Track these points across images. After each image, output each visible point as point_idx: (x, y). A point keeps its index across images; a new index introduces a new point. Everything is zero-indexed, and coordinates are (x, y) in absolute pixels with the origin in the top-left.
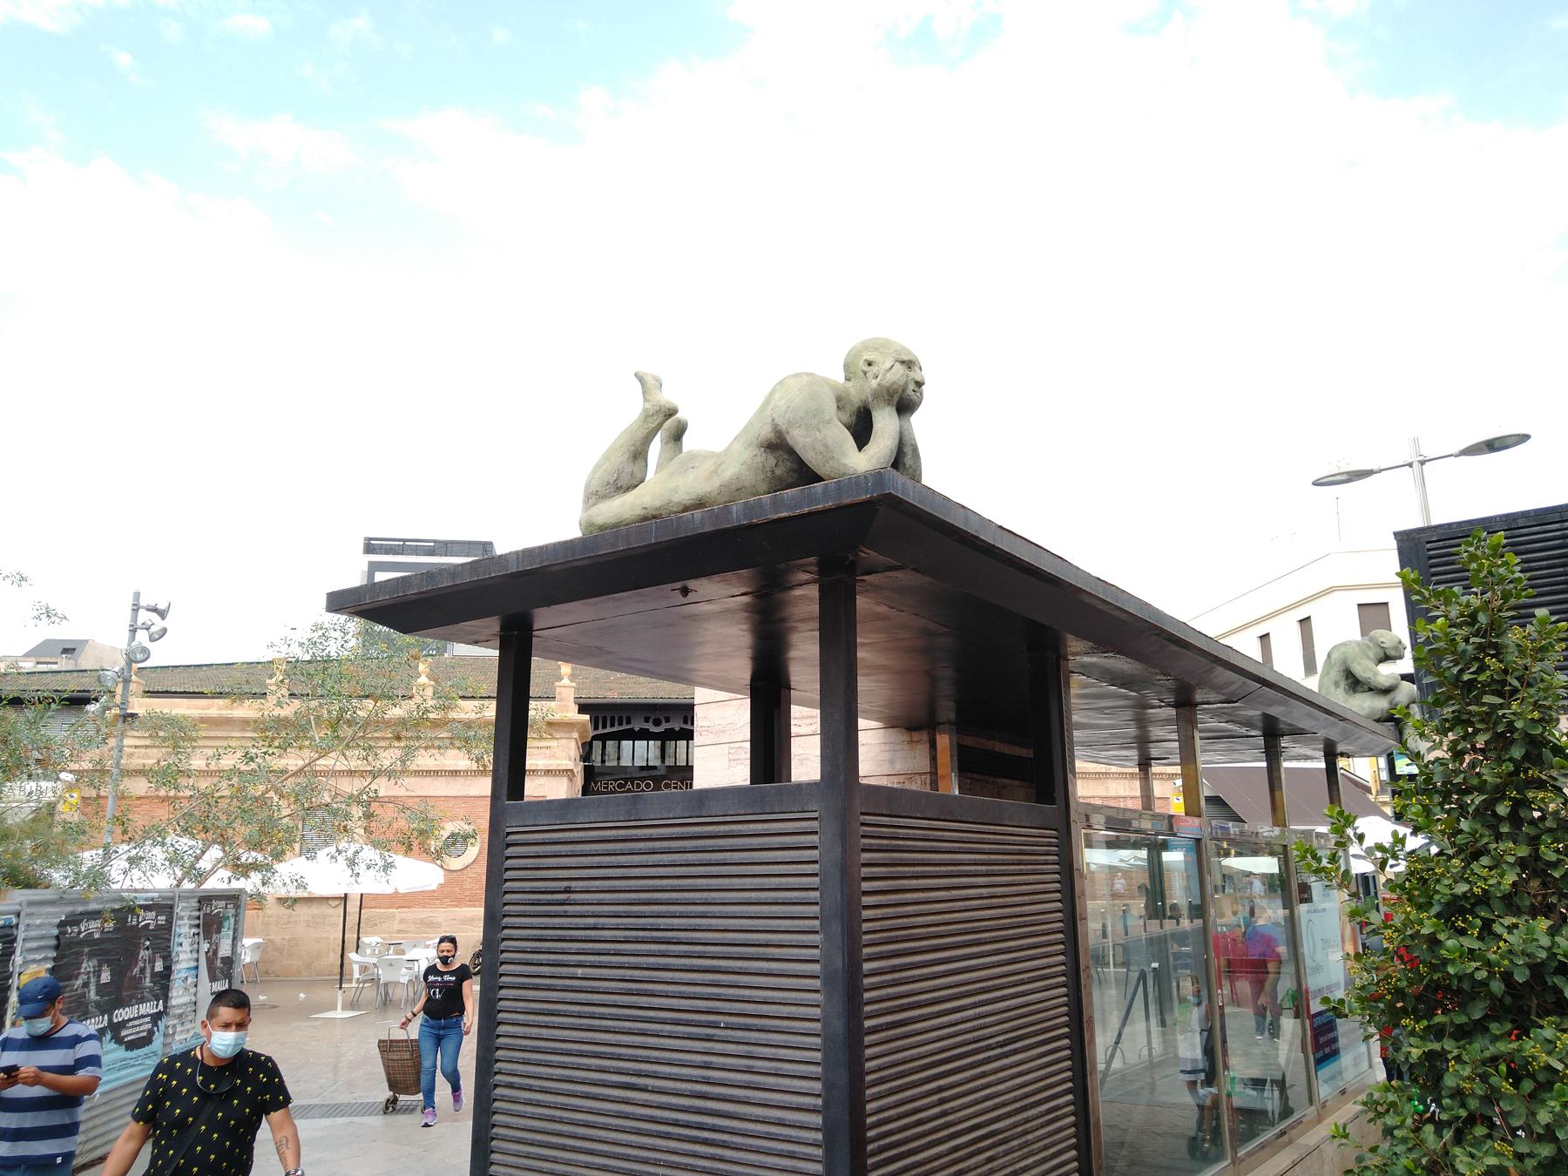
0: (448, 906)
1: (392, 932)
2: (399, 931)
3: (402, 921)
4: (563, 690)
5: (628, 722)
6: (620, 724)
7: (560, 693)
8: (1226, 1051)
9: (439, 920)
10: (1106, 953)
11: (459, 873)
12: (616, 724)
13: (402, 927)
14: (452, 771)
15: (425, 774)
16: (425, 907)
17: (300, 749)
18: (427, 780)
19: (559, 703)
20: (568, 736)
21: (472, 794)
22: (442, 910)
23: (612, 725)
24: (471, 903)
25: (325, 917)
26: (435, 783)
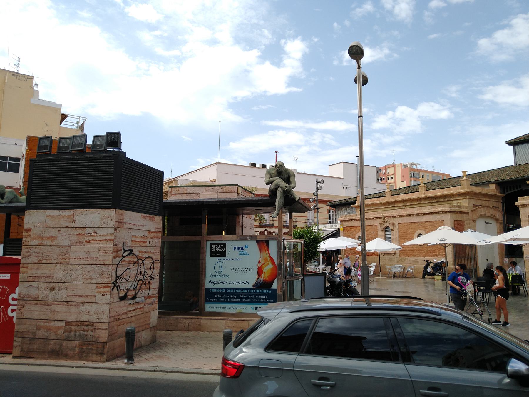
0: (421, 256)
1: (407, 264)
2: (409, 264)
3: (409, 260)
4: (463, 181)
5: (520, 187)
6: (514, 189)
7: (462, 183)
8: (144, 370)
9: (419, 260)
10: (380, 321)
11: (423, 246)
12: (512, 189)
13: (409, 262)
14: (417, 214)
15: (521, 206)
16: (415, 257)
17: (34, 239)
18: (411, 217)
19: (462, 186)
20: (465, 198)
21: (423, 221)
22: (419, 257)
23: (517, 188)
24: (427, 256)
25: (392, 258)
26: (413, 218)
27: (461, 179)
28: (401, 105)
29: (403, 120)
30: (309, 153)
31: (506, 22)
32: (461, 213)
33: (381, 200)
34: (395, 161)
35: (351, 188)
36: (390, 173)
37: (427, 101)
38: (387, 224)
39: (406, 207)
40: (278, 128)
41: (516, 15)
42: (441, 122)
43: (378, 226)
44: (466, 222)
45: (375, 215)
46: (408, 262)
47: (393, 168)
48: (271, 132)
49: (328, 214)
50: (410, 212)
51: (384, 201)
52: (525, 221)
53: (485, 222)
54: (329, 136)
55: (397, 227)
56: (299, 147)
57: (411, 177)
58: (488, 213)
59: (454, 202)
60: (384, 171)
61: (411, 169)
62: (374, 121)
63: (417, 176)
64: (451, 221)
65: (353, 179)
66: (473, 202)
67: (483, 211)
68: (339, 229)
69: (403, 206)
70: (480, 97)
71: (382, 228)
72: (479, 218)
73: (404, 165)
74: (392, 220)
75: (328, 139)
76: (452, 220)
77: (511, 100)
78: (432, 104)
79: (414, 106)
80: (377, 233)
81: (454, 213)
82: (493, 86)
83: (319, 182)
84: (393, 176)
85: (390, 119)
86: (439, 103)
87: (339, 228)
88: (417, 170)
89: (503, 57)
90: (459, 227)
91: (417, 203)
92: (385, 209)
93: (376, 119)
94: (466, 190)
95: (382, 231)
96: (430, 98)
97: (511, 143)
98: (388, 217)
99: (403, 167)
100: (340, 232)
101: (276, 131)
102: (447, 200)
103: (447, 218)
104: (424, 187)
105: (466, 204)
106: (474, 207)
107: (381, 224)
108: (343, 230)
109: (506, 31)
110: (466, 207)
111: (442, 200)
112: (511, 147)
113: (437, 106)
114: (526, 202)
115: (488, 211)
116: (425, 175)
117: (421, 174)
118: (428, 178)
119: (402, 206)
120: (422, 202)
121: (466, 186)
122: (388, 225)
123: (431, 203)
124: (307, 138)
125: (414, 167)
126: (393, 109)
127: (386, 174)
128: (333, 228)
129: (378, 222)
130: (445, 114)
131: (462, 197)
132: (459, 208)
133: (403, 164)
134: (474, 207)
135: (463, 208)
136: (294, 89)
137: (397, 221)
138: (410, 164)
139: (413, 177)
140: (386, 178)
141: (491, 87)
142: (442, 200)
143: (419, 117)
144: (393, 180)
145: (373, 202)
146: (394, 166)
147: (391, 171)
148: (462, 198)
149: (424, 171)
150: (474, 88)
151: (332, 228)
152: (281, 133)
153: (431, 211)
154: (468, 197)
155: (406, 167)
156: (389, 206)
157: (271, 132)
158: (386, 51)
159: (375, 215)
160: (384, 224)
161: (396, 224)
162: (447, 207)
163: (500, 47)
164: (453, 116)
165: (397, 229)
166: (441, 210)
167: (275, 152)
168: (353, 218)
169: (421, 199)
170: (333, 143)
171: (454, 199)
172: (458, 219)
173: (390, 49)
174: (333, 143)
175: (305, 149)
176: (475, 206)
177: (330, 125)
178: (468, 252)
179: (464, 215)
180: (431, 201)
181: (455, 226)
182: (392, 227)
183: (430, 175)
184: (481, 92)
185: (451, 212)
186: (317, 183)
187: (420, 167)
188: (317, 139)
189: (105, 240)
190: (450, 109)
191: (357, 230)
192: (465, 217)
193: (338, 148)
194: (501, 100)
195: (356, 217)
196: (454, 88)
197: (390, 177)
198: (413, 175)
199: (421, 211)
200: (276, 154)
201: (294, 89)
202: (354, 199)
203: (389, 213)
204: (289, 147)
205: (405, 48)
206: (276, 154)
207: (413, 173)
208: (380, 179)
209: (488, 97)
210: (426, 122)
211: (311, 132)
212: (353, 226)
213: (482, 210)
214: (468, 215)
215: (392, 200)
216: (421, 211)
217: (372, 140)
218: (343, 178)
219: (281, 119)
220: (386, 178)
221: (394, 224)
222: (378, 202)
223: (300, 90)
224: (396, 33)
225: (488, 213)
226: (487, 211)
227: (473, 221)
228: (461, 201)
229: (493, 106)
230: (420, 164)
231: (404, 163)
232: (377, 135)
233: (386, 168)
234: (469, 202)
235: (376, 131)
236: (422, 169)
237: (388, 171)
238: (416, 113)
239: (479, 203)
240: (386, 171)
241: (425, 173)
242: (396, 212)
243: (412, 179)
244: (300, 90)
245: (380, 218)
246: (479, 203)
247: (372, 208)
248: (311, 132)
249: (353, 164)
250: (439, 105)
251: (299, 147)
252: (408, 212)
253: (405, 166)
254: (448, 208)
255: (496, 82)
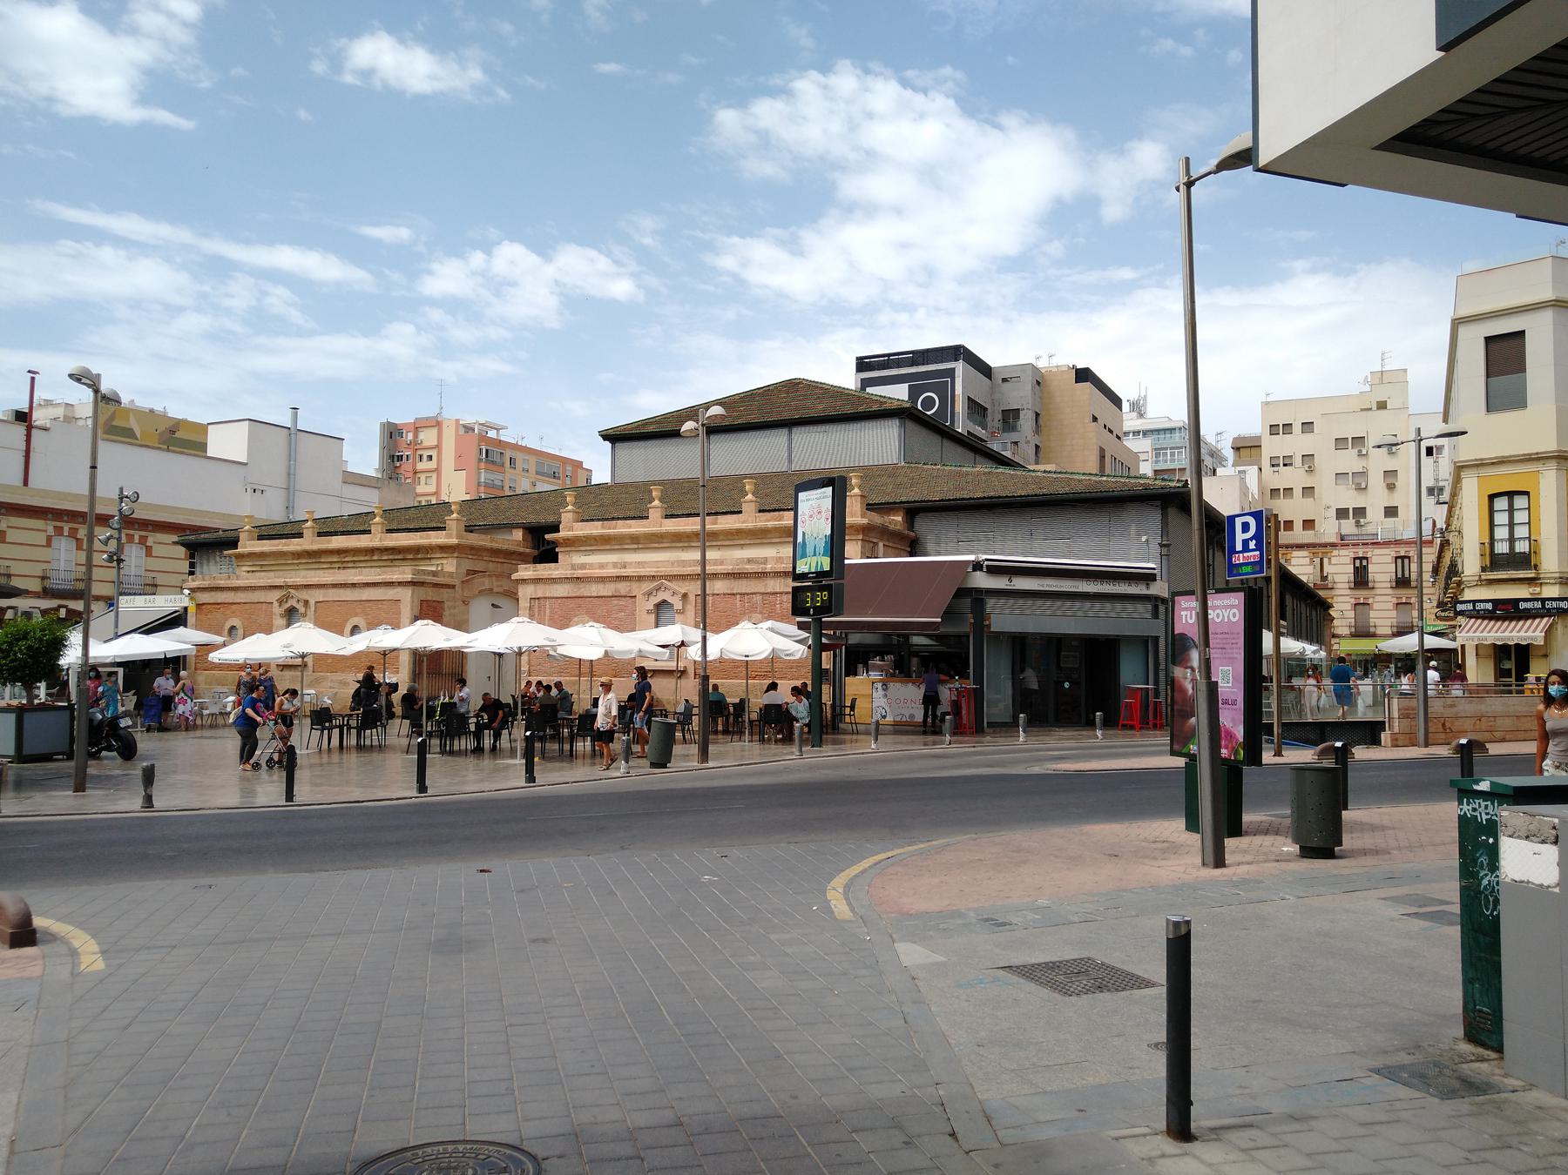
3: (332, 681)
18: (342, 591)
21: (364, 599)
27: (448, 518)
28: (513, 239)
29: (513, 284)
30: (214, 337)
31: (777, 81)
32: (436, 585)
33: (294, 545)
34: (444, 411)
35: (269, 492)
36: (425, 444)
37: (581, 242)
38: (292, 603)
39: (344, 565)
40: (100, 237)
41: (803, 69)
42: (608, 308)
43: (274, 606)
44: (447, 604)
45: (269, 581)
46: (329, 685)
47: (435, 431)
48: (67, 245)
49: (187, 563)
50: (340, 578)
51: (299, 548)
52: (525, 608)
53: (493, 605)
54: (282, 291)
55: (313, 609)
56: (174, 311)
57: (480, 460)
58: (498, 586)
59: (434, 562)
60: (410, 436)
61: (483, 438)
62: (430, 273)
63: (497, 458)
64: (413, 602)
65: (273, 473)
66: (468, 564)
67: (486, 583)
68: (186, 609)
69: (338, 562)
70: (709, 258)
71: (282, 610)
72: (477, 596)
73: (464, 426)
74: (304, 595)
75: (279, 299)
76: (416, 601)
77: (776, 280)
78: (593, 253)
79: (543, 248)
80: (272, 621)
81: (422, 586)
82: (742, 236)
83: (127, 497)
84: (434, 453)
85: (474, 273)
86: (609, 254)
87: (185, 605)
88: (500, 443)
89: (768, 169)
90: (430, 611)
91: (366, 558)
92: (301, 567)
93: (435, 266)
94: (454, 541)
95: (282, 616)
96: (591, 237)
97: (609, 436)
98: (297, 587)
99: (462, 431)
100: (189, 615)
101: (89, 244)
102: (419, 556)
103: (406, 595)
104: (380, 526)
105: (452, 569)
106: (468, 574)
107: (281, 602)
108: (194, 611)
109: (779, 105)
110: (451, 575)
111: (411, 556)
112: (608, 445)
113: (603, 263)
114: (527, 575)
115: (499, 583)
116: (519, 457)
117: (508, 454)
118: (526, 467)
119: (335, 562)
120: (375, 558)
121: (454, 533)
122: (295, 605)
123: (392, 560)
124: (206, 288)
125: (492, 434)
126: (488, 248)
127: (415, 444)
128: (171, 604)
129: (274, 596)
130: (622, 288)
131: (446, 552)
132: (434, 576)
133: (461, 423)
134: (468, 574)
135: (444, 577)
136: (164, 117)
137: (314, 596)
138: (480, 424)
139: (486, 462)
140: (415, 454)
141: (735, 240)
142: (411, 556)
143: (557, 283)
144: (432, 465)
145: (274, 549)
146: (437, 424)
147: (428, 437)
148: (445, 556)
149: (516, 447)
150: (698, 233)
151: (146, 605)
152: (107, 253)
153: (378, 579)
154: (455, 555)
155: (470, 431)
156: (310, 561)
157: (70, 243)
158: (476, 74)
159: (269, 581)
160: (286, 602)
161: (312, 602)
162: (404, 573)
163: (765, 142)
164: (641, 298)
165: (313, 613)
166: (397, 578)
167: (29, 372)
168: (220, 584)
169: (371, 551)
170: (296, 317)
171: (432, 556)
172: (430, 598)
173: (487, 69)
174: (296, 317)
175: (194, 322)
176: (469, 572)
177: (287, 258)
178: (446, 666)
179: (445, 591)
180: (391, 557)
181: (420, 613)
182: (302, 610)
183: (533, 459)
184: (710, 247)
185: (412, 583)
186: (122, 498)
187: (506, 437)
188: (240, 294)
189: (1131, 1137)
190: (635, 275)
191: (228, 612)
192: (445, 594)
193: (310, 334)
194: (755, 276)
195: (227, 581)
196: (648, 223)
197: (426, 454)
198: (487, 457)
199: (361, 577)
200: (33, 379)
201: (164, 117)
202: (232, 534)
203: (299, 577)
204: (136, 304)
205: (530, 80)
206: (33, 379)
207: (487, 451)
208: (398, 456)
209: (727, 262)
210: (574, 302)
211: (221, 269)
212: (219, 601)
213: (486, 580)
214: (452, 590)
215: (315, 547)
216: (361, 577)
217: (419, 329)
218: (246, 464)
219: (110, 209)
220: (415, 454)
221: (306, 603)
222: (285, 549)
223: (186, 124)
224: (507, 28)
225: (498, 586)
226: (495, 583)
227: (463, 602)
228: (445, 562)
229: (737, 289)
230: (506, 428)
231: (468, 419)
232: (436, 315)
233: (417, 427)
234: (458, 566)
235: (432, 302)
236: (514, 442)
237: (422, 436)
238: (550, 271)
239: (480, 566)
240: (416, 436)
241: (518, 453)
242: (312, 577)
243: (483, 465)
244: (186, 124)
245: (280, 587)
246: (480, 566)
247: (273, 563)
248: (221, 269)
249: (278, 428)
250: (610, 261)
251: (174, 311)
252: (335, 578)
253: (468, 429)
254: (409, 577)
255: (750, 227)
